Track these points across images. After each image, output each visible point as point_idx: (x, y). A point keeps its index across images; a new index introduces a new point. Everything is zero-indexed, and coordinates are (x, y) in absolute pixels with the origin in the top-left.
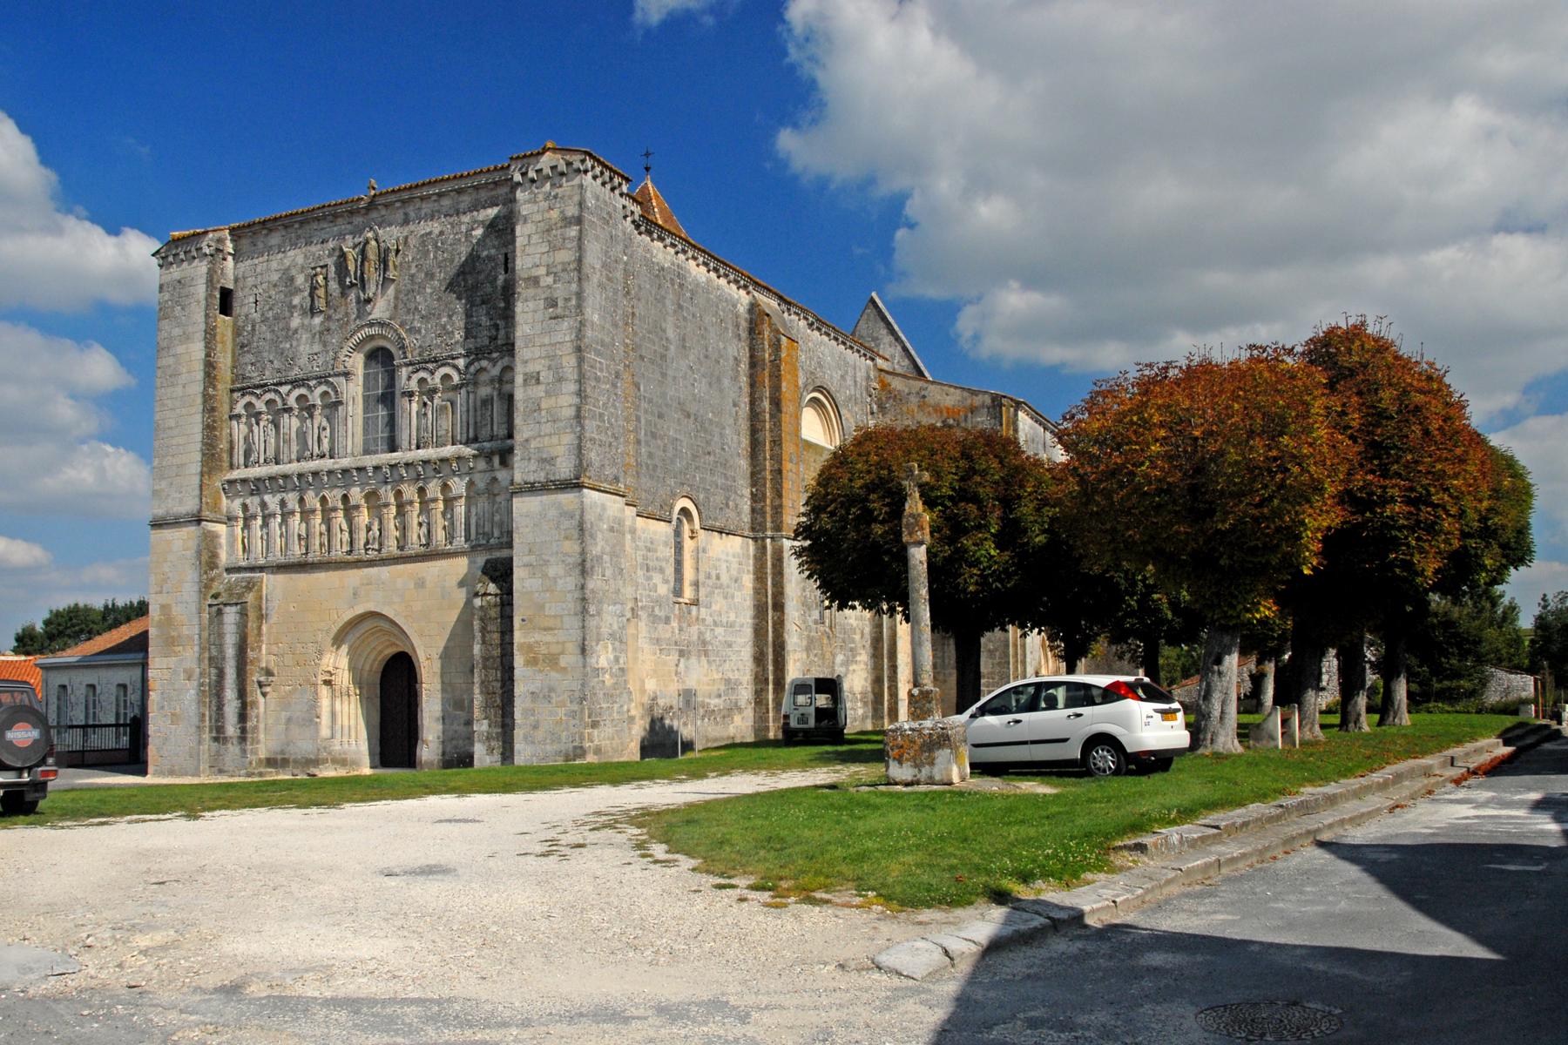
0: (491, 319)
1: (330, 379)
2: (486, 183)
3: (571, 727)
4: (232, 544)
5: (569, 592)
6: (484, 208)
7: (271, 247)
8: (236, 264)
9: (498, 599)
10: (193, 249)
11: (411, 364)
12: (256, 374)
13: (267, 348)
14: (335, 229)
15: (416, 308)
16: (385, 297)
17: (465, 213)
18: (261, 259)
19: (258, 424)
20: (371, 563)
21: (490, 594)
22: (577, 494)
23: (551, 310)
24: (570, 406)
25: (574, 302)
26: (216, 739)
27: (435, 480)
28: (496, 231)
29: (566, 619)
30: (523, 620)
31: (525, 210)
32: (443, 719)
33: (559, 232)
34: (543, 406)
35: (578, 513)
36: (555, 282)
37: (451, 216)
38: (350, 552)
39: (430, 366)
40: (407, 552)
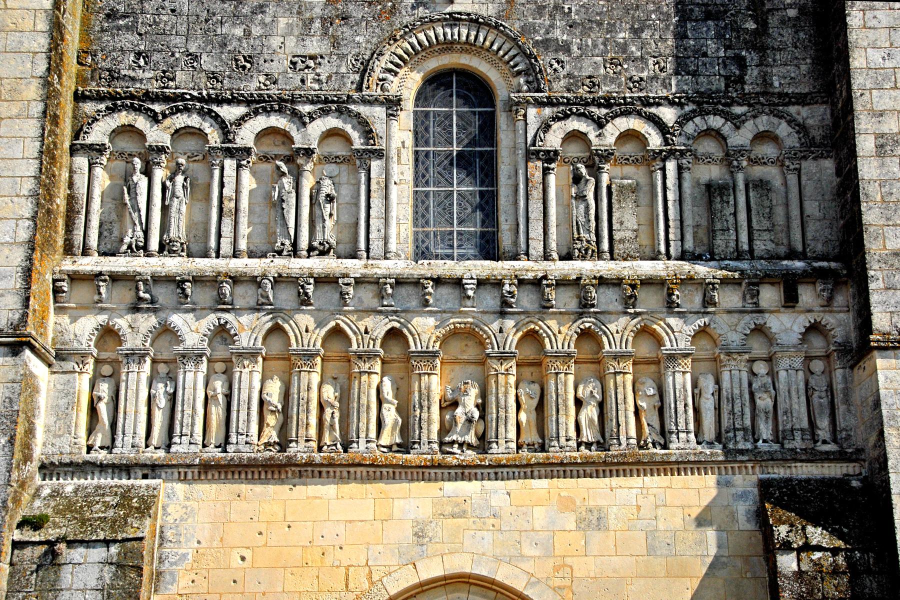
0: (727, 48)
1: (352, 107)
4: (63, 414)
9: (840, 560)
11: (550, 103)
12: (149, 75)
13: (183, 29)
19: (148, 172)
20: (464, 472)
21: (819, 548)
27: (623, 320)
38: (405, 447)
40: (554, 453)
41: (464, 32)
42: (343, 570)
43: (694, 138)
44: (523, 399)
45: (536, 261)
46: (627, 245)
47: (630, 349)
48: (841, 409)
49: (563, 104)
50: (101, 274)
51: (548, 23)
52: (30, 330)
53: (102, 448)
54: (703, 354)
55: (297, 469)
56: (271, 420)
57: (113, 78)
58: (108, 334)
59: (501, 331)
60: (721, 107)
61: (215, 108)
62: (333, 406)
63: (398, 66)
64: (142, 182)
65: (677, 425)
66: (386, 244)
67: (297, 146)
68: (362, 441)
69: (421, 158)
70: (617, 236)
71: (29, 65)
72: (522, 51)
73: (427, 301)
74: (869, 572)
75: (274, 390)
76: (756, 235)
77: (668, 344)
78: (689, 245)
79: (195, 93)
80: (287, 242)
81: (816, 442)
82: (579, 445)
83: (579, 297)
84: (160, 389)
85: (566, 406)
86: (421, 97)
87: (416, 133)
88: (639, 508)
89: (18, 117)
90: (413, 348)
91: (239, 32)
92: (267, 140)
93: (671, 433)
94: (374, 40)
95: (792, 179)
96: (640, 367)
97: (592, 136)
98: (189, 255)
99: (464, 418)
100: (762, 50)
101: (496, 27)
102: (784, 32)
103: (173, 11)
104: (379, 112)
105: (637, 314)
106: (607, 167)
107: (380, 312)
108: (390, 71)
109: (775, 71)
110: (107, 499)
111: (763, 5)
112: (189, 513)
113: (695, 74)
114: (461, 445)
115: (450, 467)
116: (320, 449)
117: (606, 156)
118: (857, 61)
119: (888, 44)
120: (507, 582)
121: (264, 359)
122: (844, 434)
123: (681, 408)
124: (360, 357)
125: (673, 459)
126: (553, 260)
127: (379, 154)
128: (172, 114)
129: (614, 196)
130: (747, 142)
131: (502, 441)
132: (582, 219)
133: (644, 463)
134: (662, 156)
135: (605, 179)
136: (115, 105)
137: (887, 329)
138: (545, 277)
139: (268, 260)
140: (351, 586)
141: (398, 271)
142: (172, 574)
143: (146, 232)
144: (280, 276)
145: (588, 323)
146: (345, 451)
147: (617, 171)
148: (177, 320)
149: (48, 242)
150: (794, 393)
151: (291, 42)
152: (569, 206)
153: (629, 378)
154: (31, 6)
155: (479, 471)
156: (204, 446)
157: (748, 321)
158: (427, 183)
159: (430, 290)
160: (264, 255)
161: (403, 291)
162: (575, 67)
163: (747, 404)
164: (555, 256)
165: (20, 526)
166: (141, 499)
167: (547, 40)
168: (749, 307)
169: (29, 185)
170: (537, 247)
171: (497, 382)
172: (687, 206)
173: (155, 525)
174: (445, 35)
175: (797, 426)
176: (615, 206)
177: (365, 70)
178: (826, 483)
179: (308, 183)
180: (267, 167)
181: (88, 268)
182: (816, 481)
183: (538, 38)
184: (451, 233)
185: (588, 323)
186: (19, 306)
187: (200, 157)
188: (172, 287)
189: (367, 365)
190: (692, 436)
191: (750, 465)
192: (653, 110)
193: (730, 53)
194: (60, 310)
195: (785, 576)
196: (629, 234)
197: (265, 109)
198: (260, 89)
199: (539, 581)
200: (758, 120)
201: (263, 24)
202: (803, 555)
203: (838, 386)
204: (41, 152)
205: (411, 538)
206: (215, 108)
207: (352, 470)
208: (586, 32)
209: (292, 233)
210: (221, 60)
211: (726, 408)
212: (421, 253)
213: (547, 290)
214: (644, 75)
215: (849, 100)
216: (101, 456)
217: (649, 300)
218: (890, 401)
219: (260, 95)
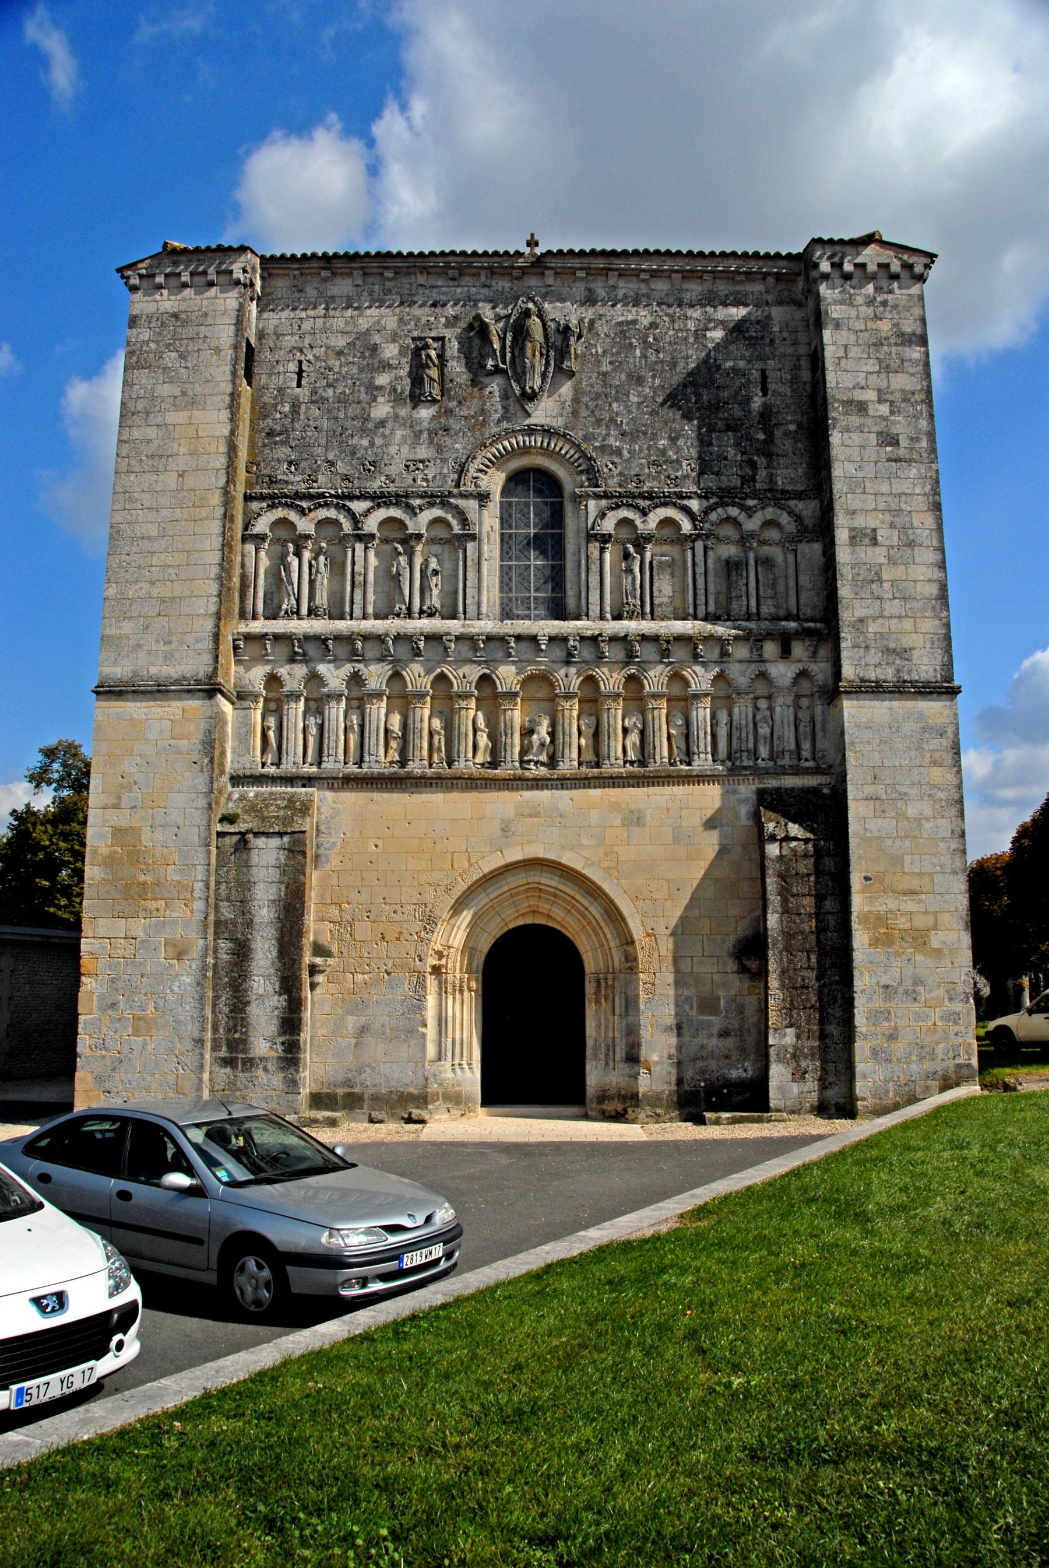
0: (743, 453)
1: (452, 500)
2: (737, 272)
3: (952, 1036)
4: (244, 737)
5: (943, 839)
6: (725, 305)
7: (333, 298)
8: (260, 312)
9: (810, 846)
10: (211, 270)
11: (606, 496)
12: (299, 478)
13: (323, 442)
14: (459, 290)
15: (612, 420)
16: (556, 397)
17: (692, 306)
18: (311, 313)
19: (298, 554)
20: (538, 783)
21: (795, 839)
22: (948, 703)
23: (889, 449)
24: (929, 581)
25: (924, 444)
26: (228, 1062)
27: (660, 668)
28: (745, 339)
29: (938, 878)
30: (867, 879)
31: (835, 312)
32: (679, 1027)
33: (894, 349)
34: (885, 576)
35: (950, 730)
36: (892, 412)
37: (669, 306)
38: (494, 764)
39: (643, 503)
40: (607, 770)
41: (539, 439)
42: (450, 855)
43: (717, 525)
44: (583, 728)
45: (594, 621)
46: (664, 608)
47: (664, 690)
48: (819, 735)
49: (616, 497)
50: (266, 634)
51: (604, 432)
52: (220, 680)
53: (272, 764)
54: (721, 693)
55: (414, 781)
56: (394, 744)
57: (272, 482)
58: (273, 680)
59: (567, 676)
60: (737, 500)
61: (348, 503)
62: (439, 734)
63: (487, 467)
64: (295, 563)
65: (698, 747)
66: (479, 607)
67: (410, 532)
68: (462, 760)
69: (506, 539)
70: (656, 601)
71: (214, 479)
72: (584, 455)
73: (510, 653)
74: (829, 855)
75: (396, 720)
76: (762, 600)
77: (693, 686)
78: (712, 608)
79: (333, 492)
80: (404, 607)
81: (800, 759)
82: (625, 762)
83: (626, 649)
84: (312, 721)
85: (616, 734)
86: (505, 491)
87: (502, 518)
88: (668, 809)
89: (206, 519)
90: (500, 690)
91: (365, 442)
92: (386, 527)
93: (694, 754)
94: (469, 447)
95: (791, 558)
96: (673, 703)
97: (638, 522)
98: (330, 618)
99: (538, 742)
100: (769, 455)
101: (565, 435)
102: (786, 442)
103: (316, 428)
104: (472, 505)
105: (671, 663)
106: (649, 546)
107: (475, 662)
108: (481, 471)
109: (779, 472)
110: (279, 802)
111: (770, 420)
112: (337, 813)
113: (718, 474)
114: (536, 763)
115: (528, 780)
116: (430, 766)
117: (649, 538)
118: (837, 471)
119: (859, 459)
120: (570, 864)
121: (388, 698)
122: (820, 754)
123: (702, 735)
124: (460, 696)
125: (695, 773)
126: (607, 620)
127: (473, 537)
128: (316, 508)
129: (655, 570)
130: (757, 528)
131: (567, 760)
132: (629, 588)
133: (673, 777)
134: (692, 539)
135: (648, 556)
136: (274, 503)
137: (852, 677)
138: (600, 635)
139: (389, 621)
140: (455, 866)
141: (488, 630)
142: (326, 856)
143: (298, 600)
144: (398, 634)
145: (633, 670)
146: (450, 768)
147: (658, 549)
148: (322, 668)
149: (229, 612)
150: (786, 724)
151: (405, 449)
152: (620, 577)
153: (664, 711)
154: (215, 434)
155: (549, 783)
156: (345, 763)
157: (753, 669)
158: (510, 559)
159: (513, 644)
160: (386, 618)
161: (492, 645)
162: (626, 468)
163: (751, 732)
164: (609, 616)
165: (221, 821)
166: (302, 802)
167: (604, 446)
168: (755, 658)
169: (215, 571)
170: (595, 610)
171: (563, 715)
172: (710, 578)
173: (312, 822)
174: (524, 442)
175: (787, 748)
176: (656, 578)
177: (462, 471)
178: (805, 791)
179: (418, 561)
180: (386, 547)
181: (257, 630)
182: (798, 789)
183: (597, 444)
184: (529, 597)
185: (633, 670)
186: (211, 662)
187: (337, 541)
188: (319, 643)
189: (465, 703)
190: (709, 756)
191: (751, 778)
192: (685, 502)
193: (745, 458)
194: (238, 662)
195: (771, 860)
196: (666, 600)
197: (385, 503)
198: (381, 487)
199: (593, 863)
200: (766, 511)
201: (384, 436)
202: (784, 844)
203: (818, 718)
204: (223, 545)
205: (499, 832)
206: (348, 503)
207: (455, 782)
208: (634, 440)
209: (407, 600)
210: (352, 465)
211: (735, 735)
212: (506, 614)
213: (602, 645)
214: (679, 474)
215: (831, 501)
216: (272, 770)
217: (680, 653)
218: (851, 732)
219: (381, 492)
